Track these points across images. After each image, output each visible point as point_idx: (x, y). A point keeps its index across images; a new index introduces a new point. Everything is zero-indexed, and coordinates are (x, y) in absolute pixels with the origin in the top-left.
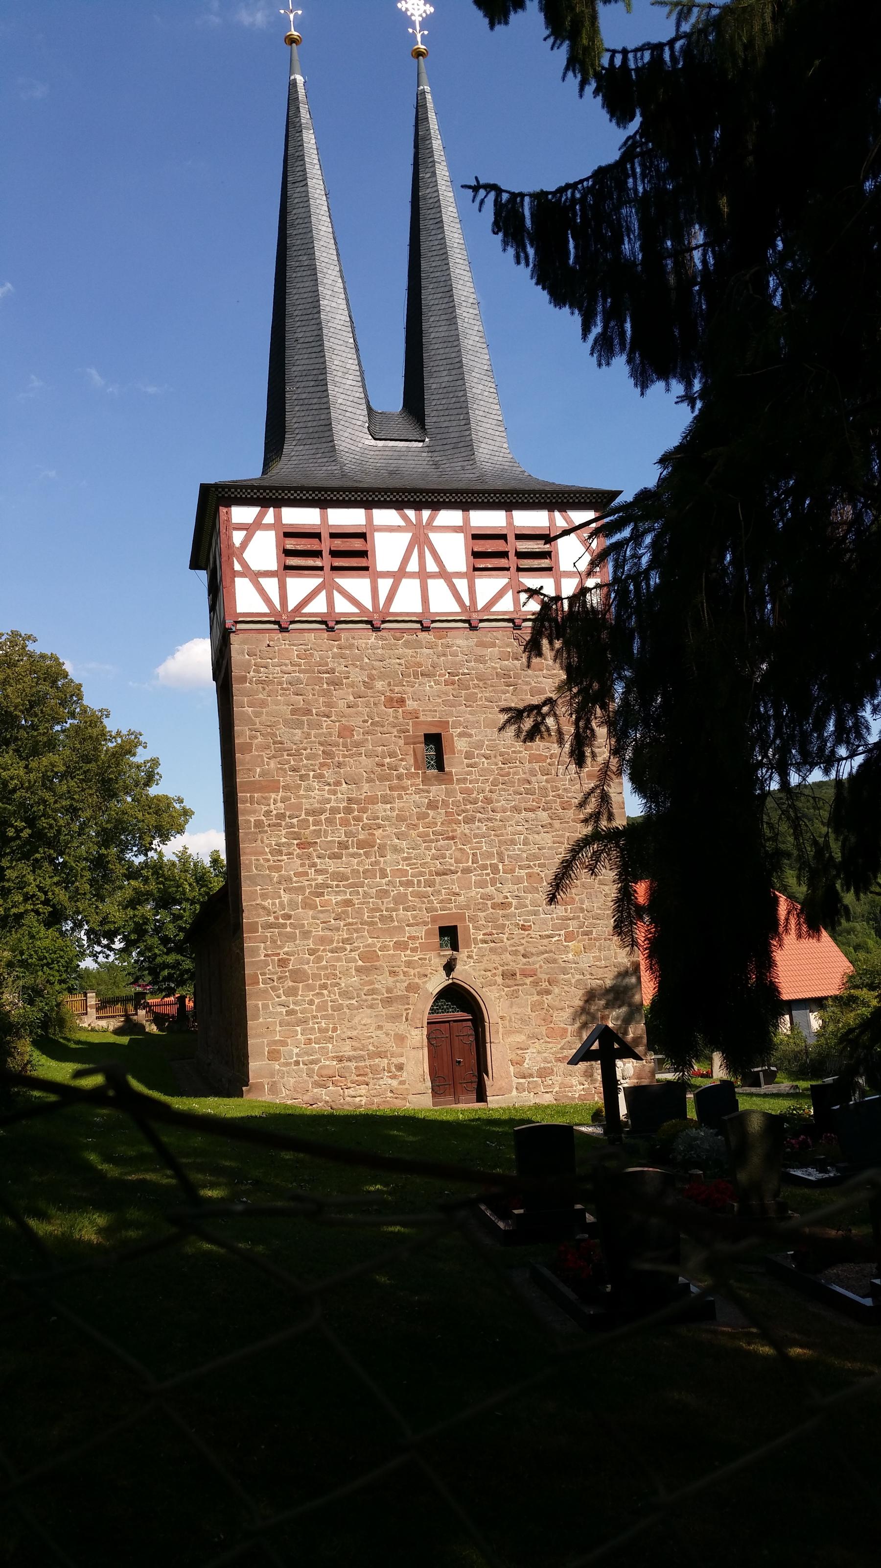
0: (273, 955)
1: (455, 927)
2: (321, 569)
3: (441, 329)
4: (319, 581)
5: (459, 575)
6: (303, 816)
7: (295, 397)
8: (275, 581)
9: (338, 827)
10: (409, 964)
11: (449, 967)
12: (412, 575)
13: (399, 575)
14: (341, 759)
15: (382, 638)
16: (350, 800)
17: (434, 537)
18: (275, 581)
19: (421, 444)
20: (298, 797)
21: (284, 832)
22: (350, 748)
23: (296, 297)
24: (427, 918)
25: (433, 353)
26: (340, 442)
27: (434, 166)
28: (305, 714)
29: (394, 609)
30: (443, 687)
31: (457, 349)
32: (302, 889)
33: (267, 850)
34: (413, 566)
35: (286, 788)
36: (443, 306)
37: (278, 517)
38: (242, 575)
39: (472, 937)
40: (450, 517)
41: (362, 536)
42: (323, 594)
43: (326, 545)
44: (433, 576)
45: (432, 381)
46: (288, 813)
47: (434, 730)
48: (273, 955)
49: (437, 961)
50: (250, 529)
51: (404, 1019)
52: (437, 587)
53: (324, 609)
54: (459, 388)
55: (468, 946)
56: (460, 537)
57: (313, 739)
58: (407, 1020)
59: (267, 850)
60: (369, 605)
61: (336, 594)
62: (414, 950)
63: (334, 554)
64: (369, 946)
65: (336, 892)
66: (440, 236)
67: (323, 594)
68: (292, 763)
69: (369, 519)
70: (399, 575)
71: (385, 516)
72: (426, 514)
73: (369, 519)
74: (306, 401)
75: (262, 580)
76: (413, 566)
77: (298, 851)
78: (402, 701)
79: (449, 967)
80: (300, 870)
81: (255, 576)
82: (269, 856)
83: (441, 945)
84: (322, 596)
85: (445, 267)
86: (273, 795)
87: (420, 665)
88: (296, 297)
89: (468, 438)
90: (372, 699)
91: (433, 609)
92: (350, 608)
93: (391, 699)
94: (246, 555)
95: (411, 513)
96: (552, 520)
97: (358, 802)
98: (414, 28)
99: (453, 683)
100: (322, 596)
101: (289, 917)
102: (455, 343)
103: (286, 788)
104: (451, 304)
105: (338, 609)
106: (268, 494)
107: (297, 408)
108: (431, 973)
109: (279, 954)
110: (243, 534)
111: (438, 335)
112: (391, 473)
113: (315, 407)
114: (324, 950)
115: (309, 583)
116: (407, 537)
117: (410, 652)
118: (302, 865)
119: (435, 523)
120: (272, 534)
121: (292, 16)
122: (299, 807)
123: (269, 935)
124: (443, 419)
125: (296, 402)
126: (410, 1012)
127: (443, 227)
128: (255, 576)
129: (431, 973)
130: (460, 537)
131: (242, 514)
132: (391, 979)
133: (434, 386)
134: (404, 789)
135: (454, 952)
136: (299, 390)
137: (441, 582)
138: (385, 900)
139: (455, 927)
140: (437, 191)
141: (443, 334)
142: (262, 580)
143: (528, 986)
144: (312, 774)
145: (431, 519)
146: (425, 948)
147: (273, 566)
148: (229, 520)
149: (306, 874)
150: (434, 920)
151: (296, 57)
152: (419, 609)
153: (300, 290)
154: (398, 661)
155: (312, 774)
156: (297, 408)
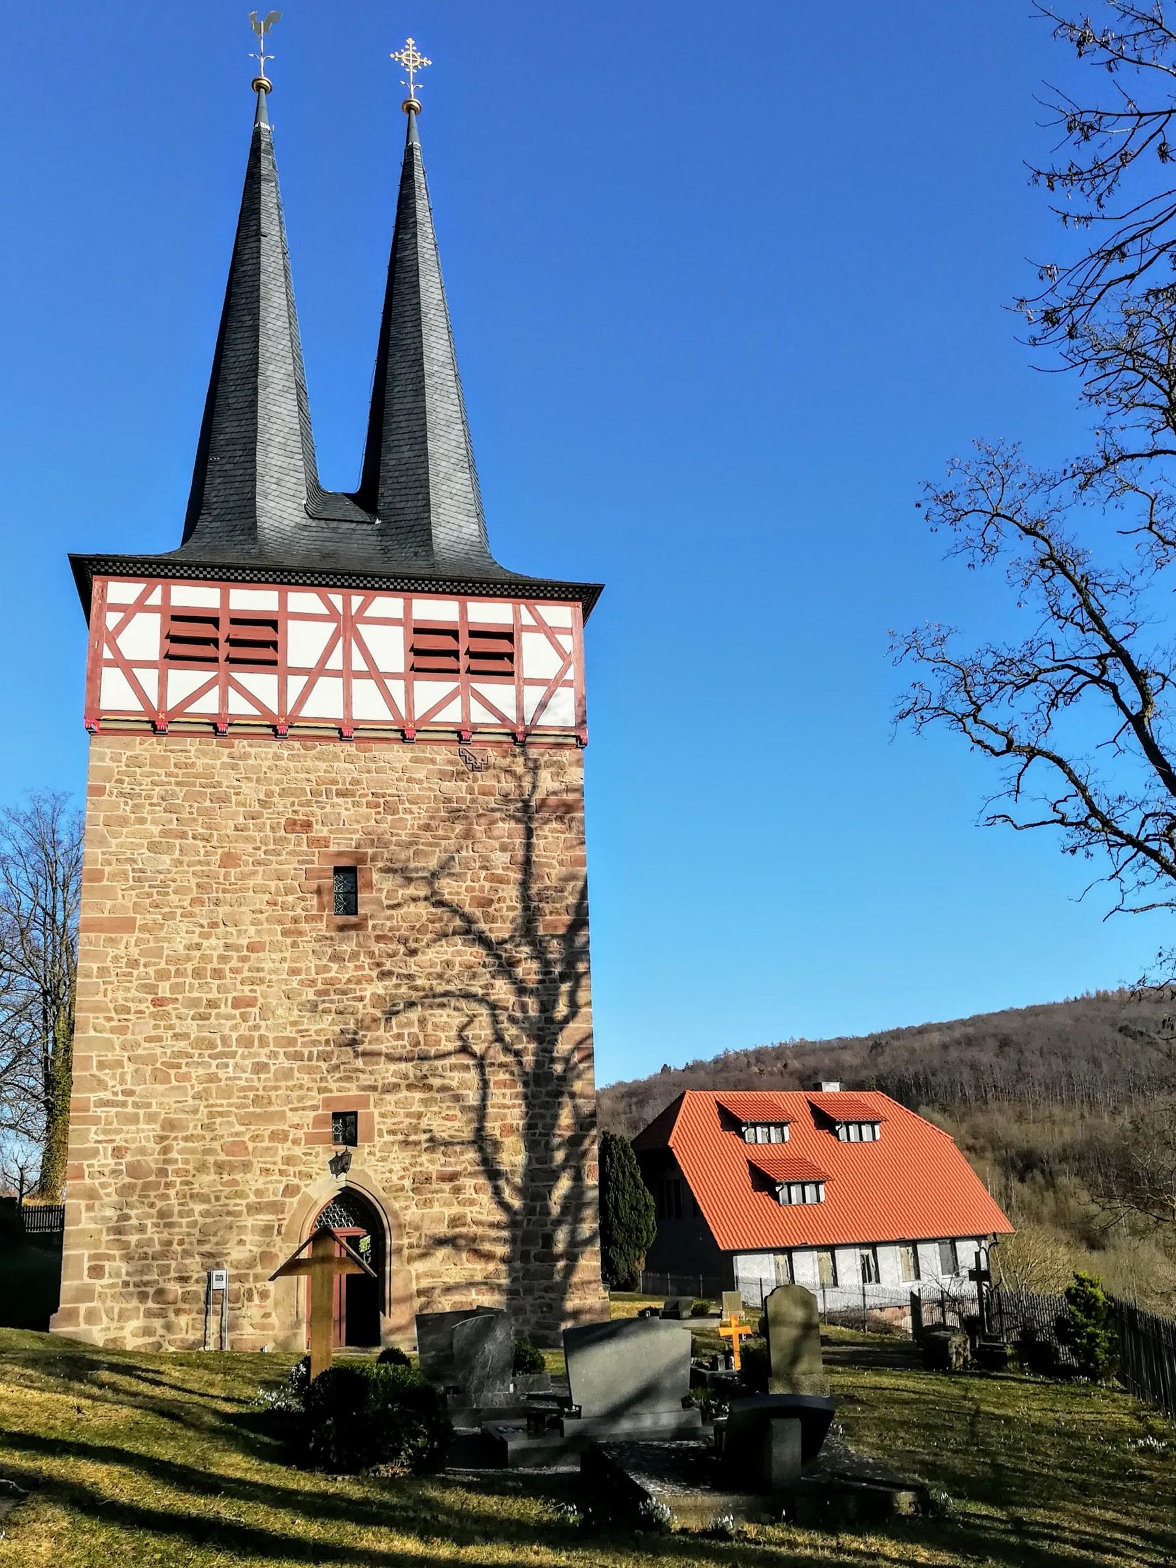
0: (106, 1141)
1: (355, 1114)
2: (215, 660)
3: (406, 400)
4: (210, 675)
5: (395, 676)
6: (163, 965)
7: (218, 468)
8: (154, 673)
9: (209, 980)
10: (288, 1160)
11: (340, 1165)
12: (335, 674)
13: (314, 674)
14: (220, 895)
15: (289, 748)
16: (227, 946)
17: (361, 628)
18: (154, 673)
19: (370, 527)
20: (157, 940)
21: (136, 983)
22: (233, 880)
23: (234, 360)
24: (317, 1098)
25: (395, 425)
26: (263, 519)
27: (415, 227)
28: (177, 837)
29: (305, 712)
30: (364, 810)
31: (421, 422)
32: (152, 1059)
33: (111, 1006)
34: (335, 662)
35: (144, 928)
36: (412, 375)
37: (166, 596)
38: (110, 664)
39: (377, 1127)
40: (388, 605)
41: (273, 624)
42: (216, 691)
43: (226, 630)
44: (360, 675)
45: (389, 456)
46: (142, 961)
47: (344, 862)
48: (106, 1141)
49: (325, 1154)
50: (129, 611)
51: (275, 1232)
52: (363, 691)
53: (214, 709)
54: (420, 465)
55: (370, 1138)
56: (400, 630)
57: (186, 868)
58: (279, 1232)
59: (111, 1006)
60: (275, 709)
61: (232, 692)
62: (296, 1142)
63: (234, 643)
64: (237, 1134)
65: (198, 1063)
66: (415, 301)
67: (216, 691)
68: (155, 896)
69: (283, 602)
70: (314, 674)
71: (303, 600)
72: (357, 600)
73: (283, 602)
74: (230, 473)
75: (137, 672)
76: (335, 662)
77: (152, 1009)
78: (308, 825)
79: (340, 1165)
80: (153, 1033)
81: (128, 667)
82: (113, 1014)
83: (336, 1138)
84: (215, 692)
85: (416, 334)
86: (126, 937)
87: (335, 782)
88: (234, 360)
89: (425, 521)
90: (269, 822)
91: (356, 716)
92: (246, 708)
93: (294, 823)
94: (121, 641)
95: (337, 599)
96: (517, 614)
97: (238, 948)
98: (407, 80)
99: (377, 806)
100: (215, 692)
101: (130, 1093)
102: (421, 416)
103: (144, 928)
104: (420, 373)
105: (232, 710)
106: (147, 569)
107: (219, 480)
108: (318, 1174)
109: (114, 1141)
110: (120, 616)
111: (402, 406)
112: (326, 556)
113: (238, 479)
114: (176, 1138)
115: (192, 678)
116: (332, 626)
117: (323, 765)
118: (156, 1027)
119: (368, 613)
120: (157, 617)
121: (262, 60)
122: (158, 953)
123: (103, 1115)
124: (398, 499)
125: (218, 474)
126: (285, 1222)
127: (418, 292)
128: (128, 667)
129: (318, 1174)
130: (400, 630)
131: (121, 591)
132: (262, 1180)
133: (393, 462)
134: (300, 933)
135: (349, 1148)
136: (224, 461)
137: (371, 684)
138: (263, 1076)
139: (355, 1114)
140: (416, 253)
141: (409, 406)
142: (137, 672)
143: (446, 1195)
144: (179, 911)
145: (364, 607)
146: (312, 1139)
147: (154, 654)
148: (103, 597)
149: (159, 1039)
150: (327, 1103)
151: (264, 103)
152: (340, 715)
153: (239, 353)
154: (307, 776)
155: (179, 911)
156: (219, 480)
